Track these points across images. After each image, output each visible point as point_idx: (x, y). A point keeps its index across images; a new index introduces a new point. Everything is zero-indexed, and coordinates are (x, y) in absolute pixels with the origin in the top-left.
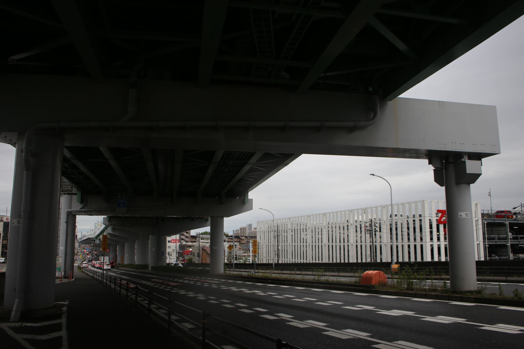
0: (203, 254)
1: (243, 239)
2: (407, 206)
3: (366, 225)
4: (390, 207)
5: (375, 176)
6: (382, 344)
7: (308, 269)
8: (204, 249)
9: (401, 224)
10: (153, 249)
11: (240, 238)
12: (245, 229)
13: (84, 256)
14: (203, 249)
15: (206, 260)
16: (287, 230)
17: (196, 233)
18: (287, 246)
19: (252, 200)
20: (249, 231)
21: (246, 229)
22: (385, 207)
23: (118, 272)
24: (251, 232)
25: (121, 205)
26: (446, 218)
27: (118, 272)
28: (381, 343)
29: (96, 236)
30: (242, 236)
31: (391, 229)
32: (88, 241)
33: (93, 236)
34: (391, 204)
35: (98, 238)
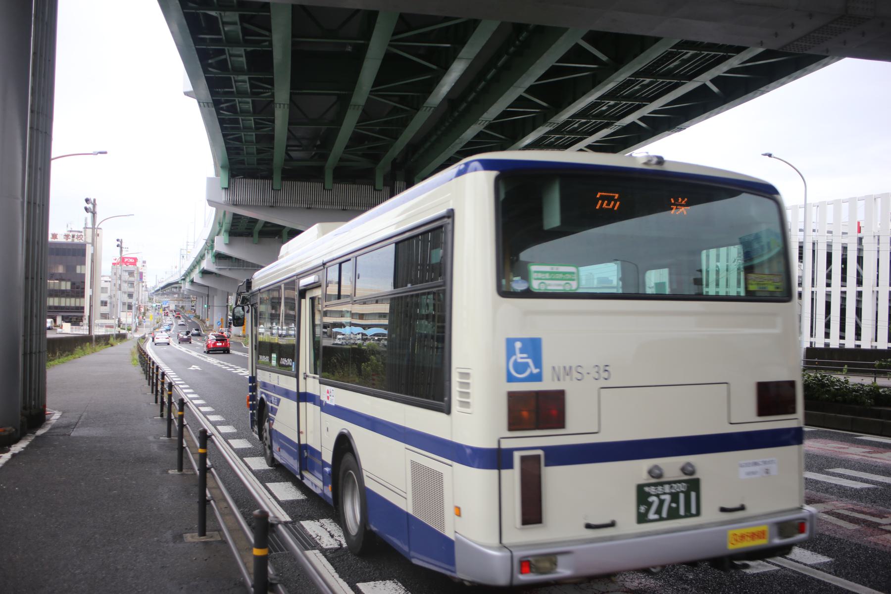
3: (802, 233)
4: (802, 211)
5: (774, 157)
6: (809, 563)
9: (814, 244)
26: (273, 367)
32: (168, 291)
33: (176, 278)
34: (803, 203)
35: (188, 280)
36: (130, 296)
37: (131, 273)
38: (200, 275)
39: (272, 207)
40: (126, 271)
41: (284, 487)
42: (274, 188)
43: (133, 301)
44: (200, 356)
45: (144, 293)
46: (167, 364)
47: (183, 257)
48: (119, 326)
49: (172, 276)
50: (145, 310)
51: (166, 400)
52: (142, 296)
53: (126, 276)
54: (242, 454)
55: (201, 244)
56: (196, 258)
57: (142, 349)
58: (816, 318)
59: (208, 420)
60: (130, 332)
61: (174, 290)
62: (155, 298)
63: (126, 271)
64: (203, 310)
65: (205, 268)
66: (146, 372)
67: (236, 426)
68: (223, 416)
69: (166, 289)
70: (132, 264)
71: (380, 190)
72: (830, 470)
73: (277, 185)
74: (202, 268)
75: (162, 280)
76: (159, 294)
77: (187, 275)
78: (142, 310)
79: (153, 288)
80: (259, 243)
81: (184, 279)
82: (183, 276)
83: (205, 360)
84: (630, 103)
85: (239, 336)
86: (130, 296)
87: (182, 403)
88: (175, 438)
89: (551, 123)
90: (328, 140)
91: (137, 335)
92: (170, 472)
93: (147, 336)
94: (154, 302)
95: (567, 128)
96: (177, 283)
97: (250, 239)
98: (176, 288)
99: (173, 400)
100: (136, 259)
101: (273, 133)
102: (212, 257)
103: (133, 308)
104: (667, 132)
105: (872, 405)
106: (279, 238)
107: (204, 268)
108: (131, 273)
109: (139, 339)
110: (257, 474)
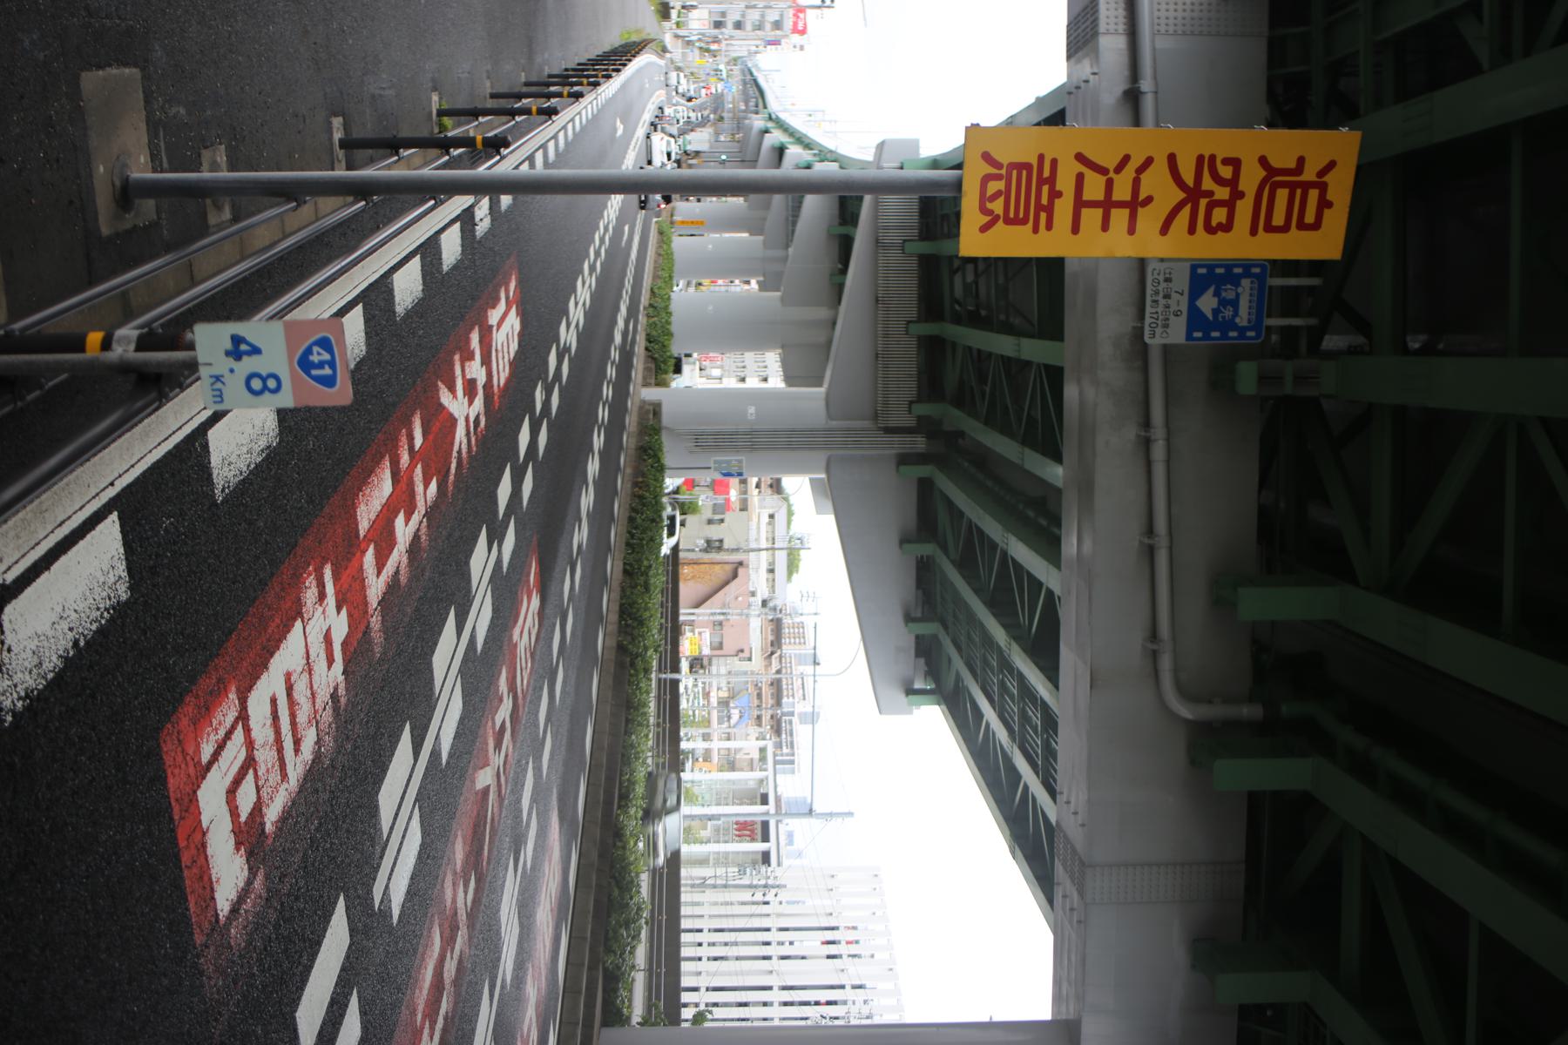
0: (717, 567)
1: (771, 664)
7: (661, 720)
8: (741, 571)
10: (752, 410)
11: (772, 653)
12: (802, 640)
14: (741, 564)
15: (693, 577)
16: (845, 1003)
17: (809, 535)
18: (765, 1004)
20: (795, 655)
21: (800, 643)
23: (626, 228)
24: (790, 663)
25: (1207, 303)
27: (626, 228)
29: (777, 117)
30: (780, 661)
33: (774, 105)
34: (778, 776)
35: (770, 125)
36: (738, 25)
37: (777, 25)
38: (777, 144)
39: (877, 241)
40: (782, 16)
41: (413, 285)
42: (907, 243)
43: (729, 30)
44: (637, 140)
45: (745, 48)
46: (624, 86)
47: (810, 115)
48: (683, 7)
49: (777, 98)
50: (715, 51)
51: (552, 89)
52: (739, 46)
53: (772, 16)
54: (429, 250)
55: (829, 143)
56: (805, 135)
57: (643, 48)
58: (725, 1020)
59: (548, 141)
60: (674, 26)
61: (752, 103)
62: (737, 69)
63: (782, 16)
64: (717, 154)
65: (787, 151)
66: (614, 52)
67: (420, 309)
68: (455, 267)
69: (755, 89)
70: (795, 24)
71: (910, 412)
72: (535, 809)
73: (910, 247)
74: (789, 146)
75: (770, 80)
76: (745, 76)
77: (777, 123)
78: (714, 47)
79: (756, 66)
80: (830, 236)
81: (770, 118)
82: (777, 116)
83: (631, 147)
84: (1040, 752)
85: (672, 215)
86: (738, 25)
87: (551, 112)
88: (490, 104)
89: (1010, 645)
90: (976, 320)
91: (668, 39)
92: (523, 74)
93: (668, 55)
94: (729, 68)
95: (1030, 708)
96: (765, 107)
97: (837, 221)
98: (757, 106)
99: (553, 100)
100: (803, 32)
101: (1034, 262)
102: (806, 161)
103: (717, 31)
104: (1008, 833)
105: (604, 964)
106: (840, 269)
107: (787, 148)
108: (777, 25)
109: (662, 41)
110: (382, 288)
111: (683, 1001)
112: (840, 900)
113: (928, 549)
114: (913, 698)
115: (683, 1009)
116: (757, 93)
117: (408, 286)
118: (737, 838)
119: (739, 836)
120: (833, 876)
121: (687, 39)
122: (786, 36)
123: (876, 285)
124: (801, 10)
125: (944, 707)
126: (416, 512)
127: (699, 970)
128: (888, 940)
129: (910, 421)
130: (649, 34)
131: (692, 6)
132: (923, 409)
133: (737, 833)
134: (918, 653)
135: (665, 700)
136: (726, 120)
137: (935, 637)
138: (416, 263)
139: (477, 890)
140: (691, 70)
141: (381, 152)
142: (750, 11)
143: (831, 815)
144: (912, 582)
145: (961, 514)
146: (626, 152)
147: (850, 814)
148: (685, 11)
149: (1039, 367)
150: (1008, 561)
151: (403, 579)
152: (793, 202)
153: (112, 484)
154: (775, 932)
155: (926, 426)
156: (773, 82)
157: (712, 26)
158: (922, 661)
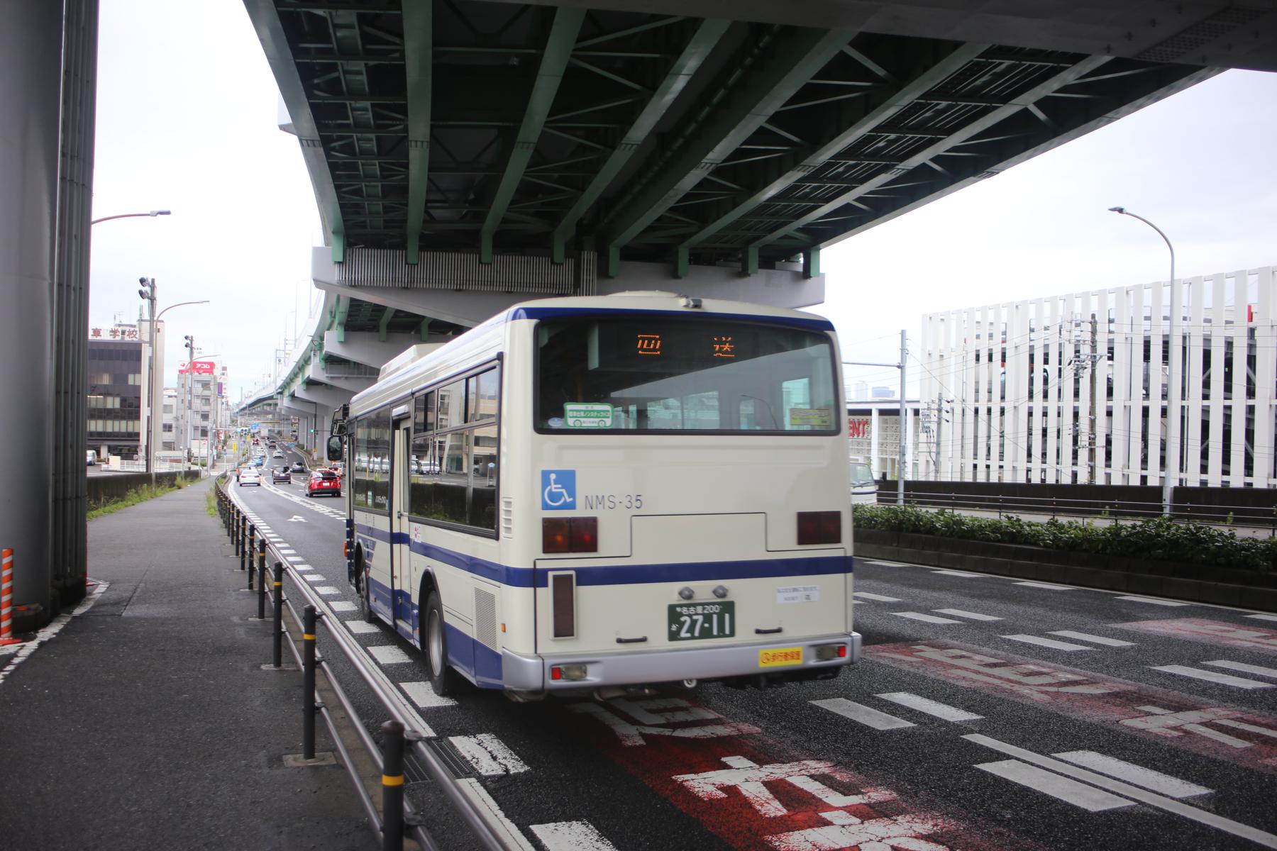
2: (1208, 286)
5: (1127, 214)
9: (1184, 338)
13: (245, 447)
19: (824, 274)
22: (1131, 293)
28: (1009, 757)
31: (1032, 357)
33: (270, 391)
34: (1170, 280)
35: (287, 393)
36: (205, 417)
37: (206, 385)
38: (304, 387)
39: (406, 288)
40: (198, 381)
43: (209, 425)
44: (304, 501)
45: (224, 413)
46: (258, 513)
47: (280, 361)
51: (256, 565)
52: (222, 417)
53: (198, 389)
60: (205, 468)
61: (268, 408)
63: (198, 381)
65: (311, 377)
66: (228, 525)
71: (561, 264)
75: (250, 394)
77: (285, 387)
78: (222, 438)
79: (237, 405)
80: (387, 340)
81: (281, 393)
86: (205, 417)
88: (270, 619)
91: (215, 473)
93: (228, 474)
96: (271, 398)
98: (270, 405)
100: (212, 365)
103: (209, 434)
104: (972, 178)
106: (416, 333)
108: (206, 385)
111: (1039, 482)
112: (952, 349)
113: (683, 254)
114: (813, 272)
115: (1032, 482)
116: (260, 404)
117: (390, 655)
118: (866, 435)
119: (864, 433)
120: (930, 354)
121: (215, 458)
122: (215, 378)
123: (446, 290)
124: (194, 365)
125: (822, 245)
126: (790, 780)
127: (1011, 468)
128: (953, 314)
129: (570, 263)
130: (211, 489)
131: (188, 453)
132: (559, 253)
133: (861, 435)
134: (773, 267)
135: (957, 498)
136: (281, 429)
137: (761, 250)
138: (349, 623)
139: (1154, 704)
140: (241, 455)
141: (283, 643)
142: (193, 407)
143: (903, 349)
144: (710, 269)
145: (659, 219)
146: (317, 513)
147: (903, 333)
148: (193, 459)
149: (551, 122)
150: (725, 166)
151: (926, 827)
152: (354, 374)
153: (405, 705)
154: (979, 403)
155: (574, 250)
156: (251, 392)
157: (205, 438)
158: (777, 264)
